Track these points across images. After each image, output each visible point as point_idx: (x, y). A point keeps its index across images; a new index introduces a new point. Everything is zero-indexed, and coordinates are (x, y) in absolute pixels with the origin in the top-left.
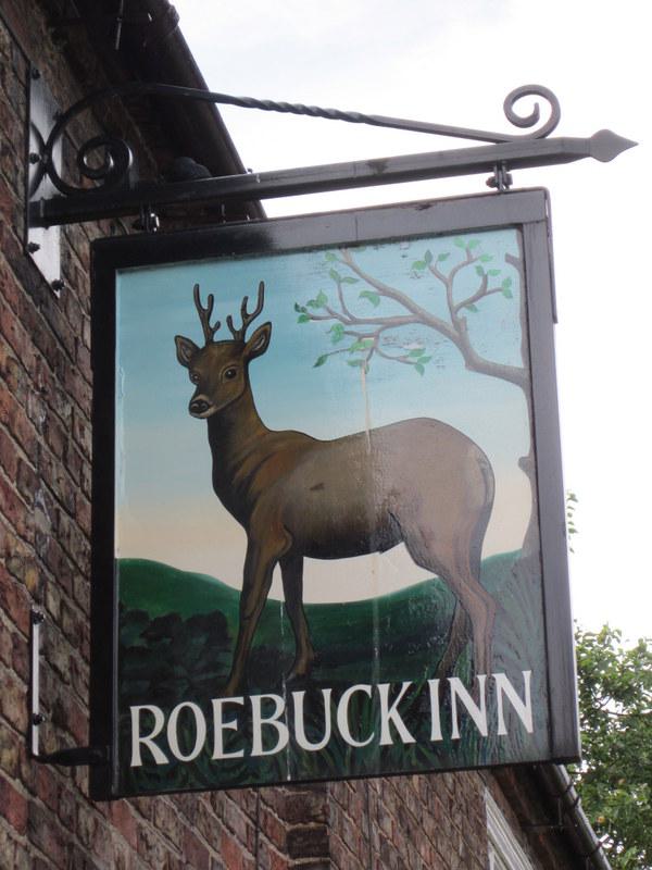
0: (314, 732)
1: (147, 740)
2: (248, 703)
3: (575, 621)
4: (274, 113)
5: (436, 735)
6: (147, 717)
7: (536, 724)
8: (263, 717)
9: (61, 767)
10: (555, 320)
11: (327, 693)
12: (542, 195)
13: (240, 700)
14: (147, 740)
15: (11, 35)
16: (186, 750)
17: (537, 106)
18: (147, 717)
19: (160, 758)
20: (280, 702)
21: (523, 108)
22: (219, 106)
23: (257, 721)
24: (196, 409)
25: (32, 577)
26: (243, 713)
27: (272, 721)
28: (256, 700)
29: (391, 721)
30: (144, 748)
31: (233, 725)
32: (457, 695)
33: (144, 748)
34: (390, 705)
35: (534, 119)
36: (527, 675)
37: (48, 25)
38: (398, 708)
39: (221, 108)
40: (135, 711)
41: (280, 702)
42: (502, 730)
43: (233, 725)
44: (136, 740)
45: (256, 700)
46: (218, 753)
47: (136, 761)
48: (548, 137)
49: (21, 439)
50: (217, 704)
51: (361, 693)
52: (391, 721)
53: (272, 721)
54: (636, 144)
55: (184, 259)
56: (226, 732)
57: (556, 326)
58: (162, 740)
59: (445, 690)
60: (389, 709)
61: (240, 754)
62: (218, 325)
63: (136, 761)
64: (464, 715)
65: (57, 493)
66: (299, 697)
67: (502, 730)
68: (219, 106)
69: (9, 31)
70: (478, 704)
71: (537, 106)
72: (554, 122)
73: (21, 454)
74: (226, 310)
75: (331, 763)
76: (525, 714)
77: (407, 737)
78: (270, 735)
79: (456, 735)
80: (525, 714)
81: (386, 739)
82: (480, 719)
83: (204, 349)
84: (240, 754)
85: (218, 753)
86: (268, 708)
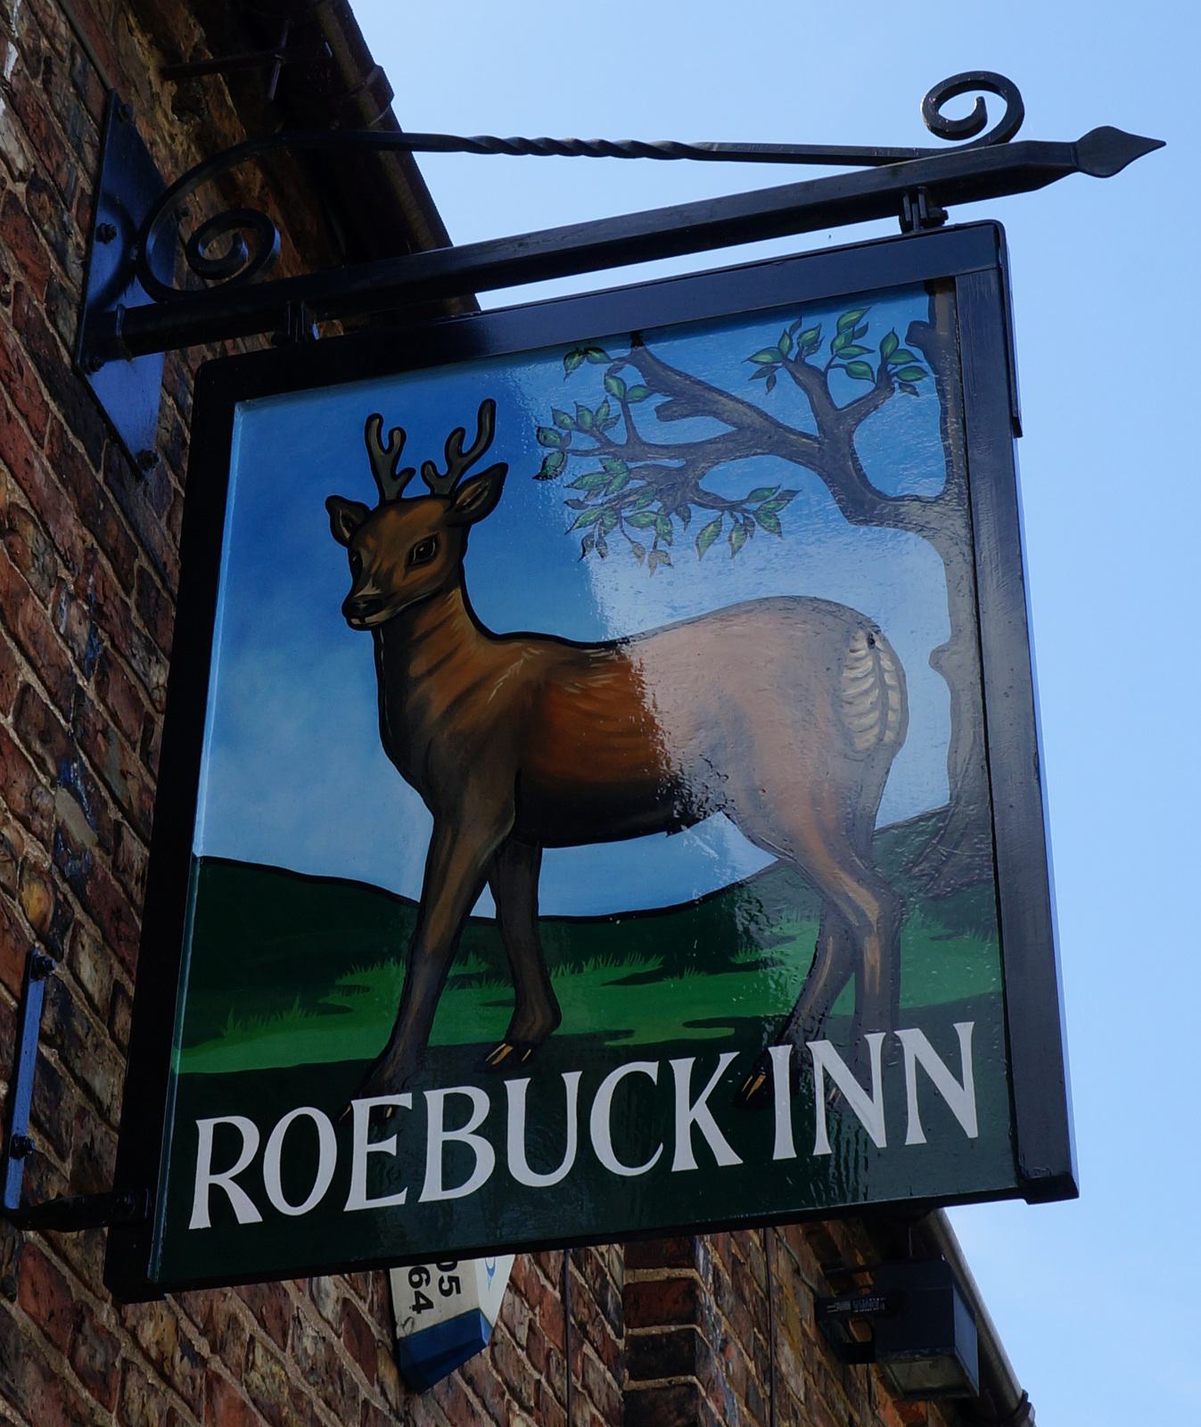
0: (543, 1153)
1: (224, 1180)
2: (420, 1103)
3: (965, 1026)
4: (583, 159)
5: (784, 1148)
6: (227, 1144)
7: (816, 1338)
8: (446, 1128)
9: (53, 1233)
10: (1019, 433)
11: (572, 1080)
12: (995, 230)
13: (405, 1100)
14: (224, 1180)
15: (69, 21)
16: (295, 1194)
17: (981, 102)
18: (227, 1144)
19: (246, 1212)
20: (481, 1102)
21: (958, 108)
22: (420, 158)
23: (436, 1137)
24: (353, 611)
25: (36, 899)
26: (410, 1126)
27: (463, 1135)
28: (435, 1100)
29: (695, 1127)
30: (217, 1194)
31: (390, 1146)
32: (919, 1065)
33: (217, 1194)
34: (693, 1102)
35: (979, 118)
36: (965, 1030)
37: (165, 75)
38: (710, 1103)
39: (425, 161)
40: (206, 1128)
41: (481, 1102)
42: (915, 1134)
43: (390, 1146)
44: (204, 1178)
45: (435, 1100)
46: (357, 1200)
47: (200, 1218)
48: (1013, 140)
49: (32, 652)
50: (361, 1109)
51: (639, 1078)
52: (695, 1127)
53: (463, 1135)
54: (1163, 144)
55: (336, 382)
56: (372, 1157)
57: (1020, 443)
58: (252, 1181)
59: (801, 1067)
60: (692, 1105)
61: (399, 1199)
62: (410, 473)
63: (200, 1218)
64: (839, 1108)
65: (118, 793)
66: (517, 1090)
67: (915, 1134)
68: (420, 158)
69: (68, 19)
70: (958, 1075)
71: (981, 102)
72: (1016, 115)
73: (27, 675)
74: (424, 450)
75: (192, 1333)
76: (963, 1103)
77: (726, 1156)
78: (458, 1162)
79: (822, 1147)
80: (963, 1103)
81: (684, 1160)
82: (870, 1113)
83: (376, 510)
84: (399, 1199)
85: (357, 1200)
86: (457, 1112)
